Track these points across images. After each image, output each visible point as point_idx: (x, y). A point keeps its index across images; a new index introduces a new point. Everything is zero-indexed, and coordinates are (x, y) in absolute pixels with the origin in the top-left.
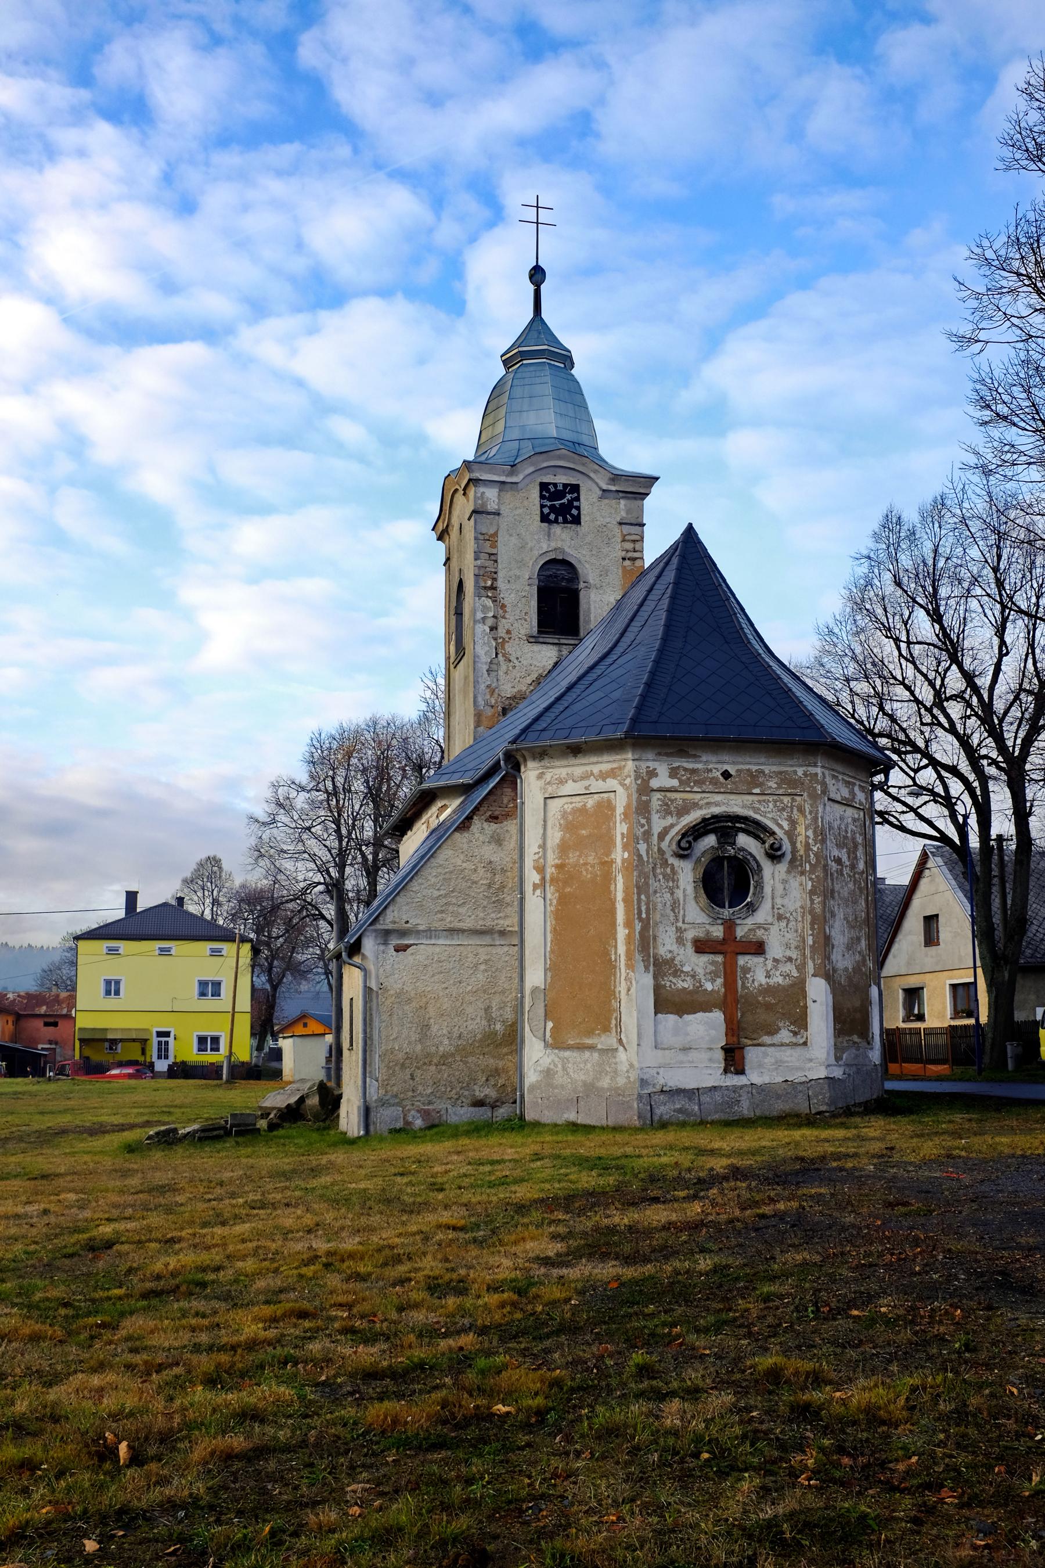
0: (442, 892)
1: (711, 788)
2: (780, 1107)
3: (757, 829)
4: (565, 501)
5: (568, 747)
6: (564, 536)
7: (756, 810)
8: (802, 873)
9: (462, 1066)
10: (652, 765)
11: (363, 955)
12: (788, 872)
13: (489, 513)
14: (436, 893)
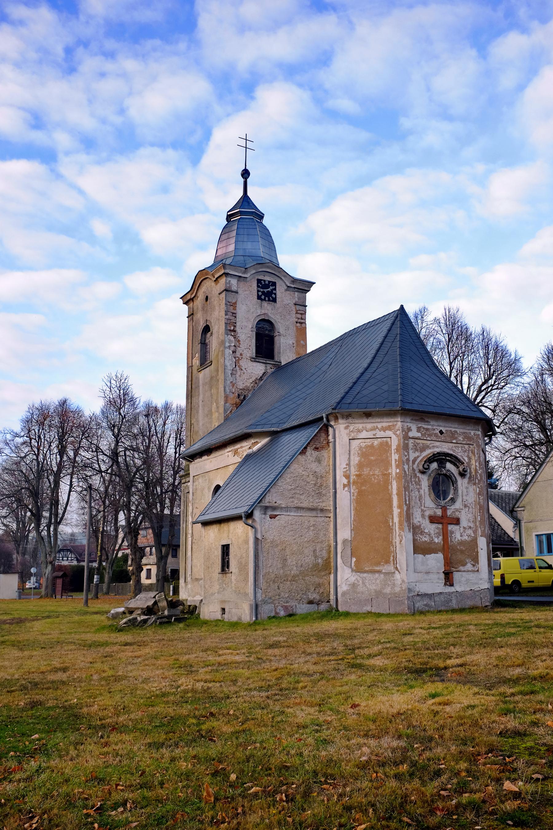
0: (293, 487)
1: (435, 438)
2: (469, 603)
3: (456, 461)
4: (269, 290)
5: (364, 413)
6: (268, 307)
7: (454, 451)
8: (475, 484)
9: (303, 582)
10: (410, 425)
11: (254, 519)
12: (468, 483)
13: (232, 292)
14: (290, 487)
